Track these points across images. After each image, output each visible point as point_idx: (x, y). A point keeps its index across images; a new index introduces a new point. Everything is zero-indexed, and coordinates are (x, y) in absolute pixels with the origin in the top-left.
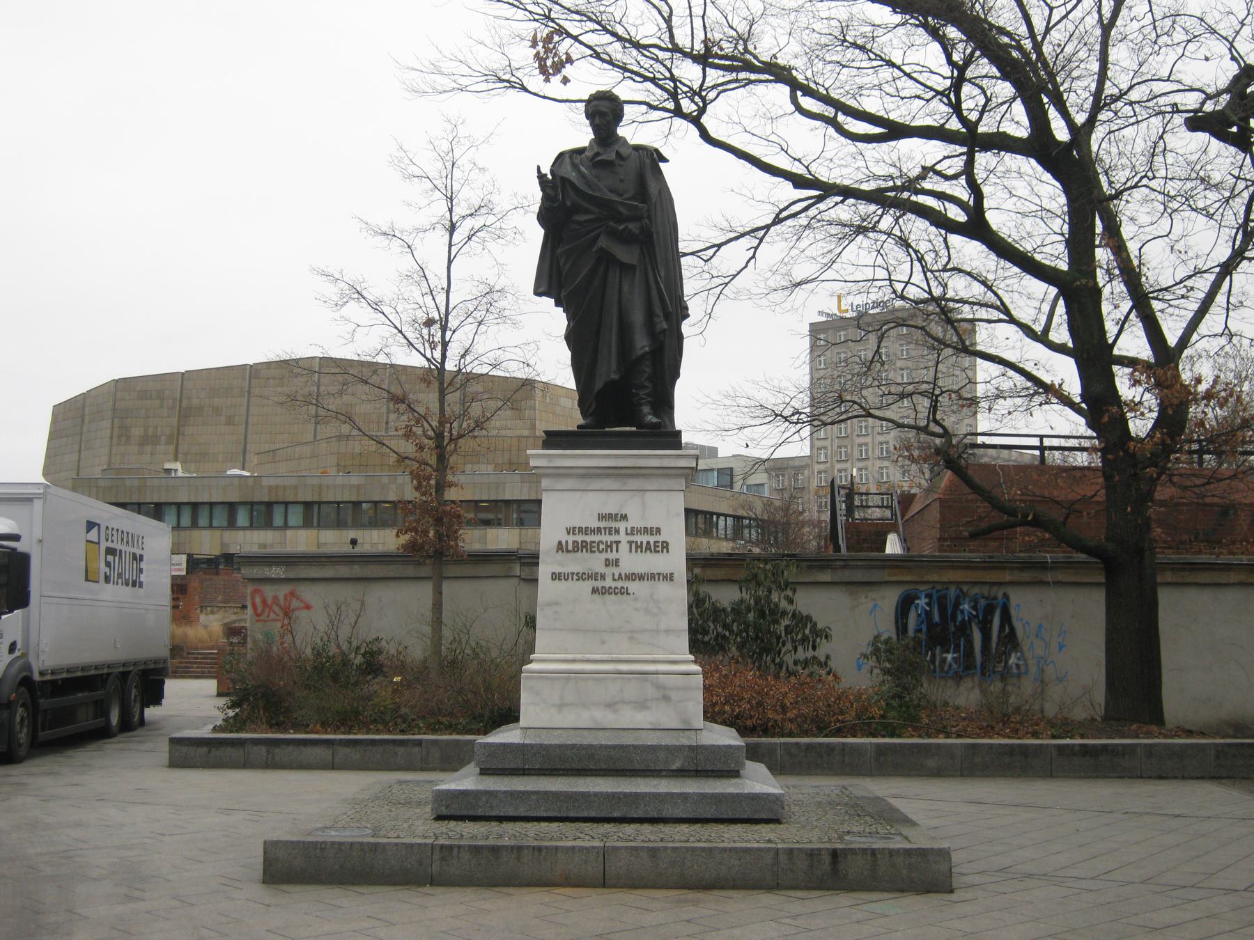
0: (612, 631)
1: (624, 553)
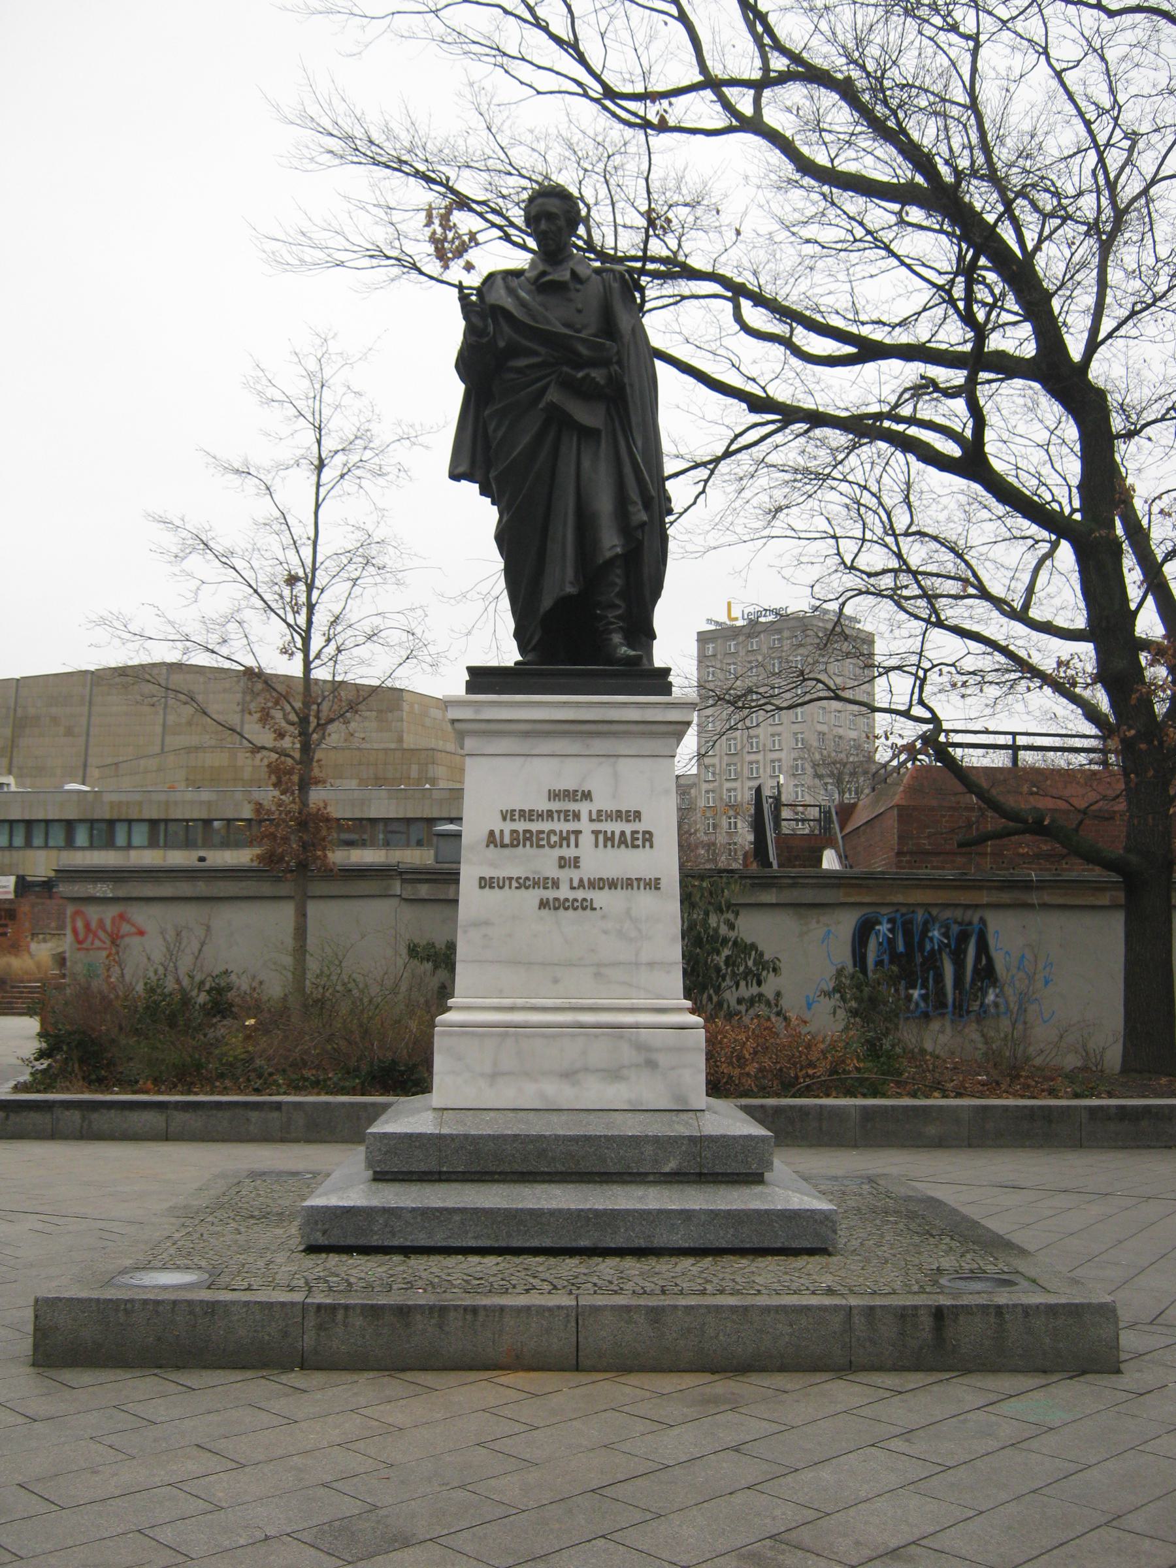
0: (570, 964)
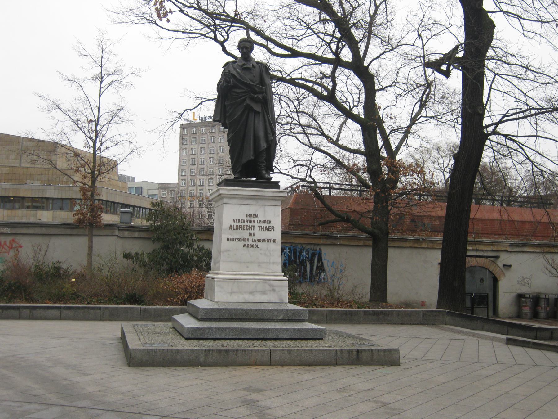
0: (252, 262)
1: (256, 231)
